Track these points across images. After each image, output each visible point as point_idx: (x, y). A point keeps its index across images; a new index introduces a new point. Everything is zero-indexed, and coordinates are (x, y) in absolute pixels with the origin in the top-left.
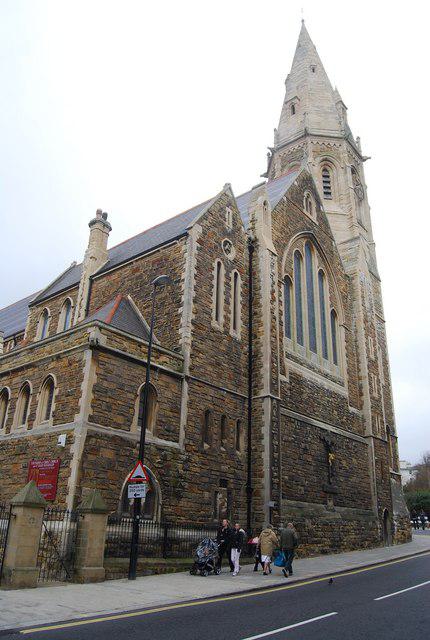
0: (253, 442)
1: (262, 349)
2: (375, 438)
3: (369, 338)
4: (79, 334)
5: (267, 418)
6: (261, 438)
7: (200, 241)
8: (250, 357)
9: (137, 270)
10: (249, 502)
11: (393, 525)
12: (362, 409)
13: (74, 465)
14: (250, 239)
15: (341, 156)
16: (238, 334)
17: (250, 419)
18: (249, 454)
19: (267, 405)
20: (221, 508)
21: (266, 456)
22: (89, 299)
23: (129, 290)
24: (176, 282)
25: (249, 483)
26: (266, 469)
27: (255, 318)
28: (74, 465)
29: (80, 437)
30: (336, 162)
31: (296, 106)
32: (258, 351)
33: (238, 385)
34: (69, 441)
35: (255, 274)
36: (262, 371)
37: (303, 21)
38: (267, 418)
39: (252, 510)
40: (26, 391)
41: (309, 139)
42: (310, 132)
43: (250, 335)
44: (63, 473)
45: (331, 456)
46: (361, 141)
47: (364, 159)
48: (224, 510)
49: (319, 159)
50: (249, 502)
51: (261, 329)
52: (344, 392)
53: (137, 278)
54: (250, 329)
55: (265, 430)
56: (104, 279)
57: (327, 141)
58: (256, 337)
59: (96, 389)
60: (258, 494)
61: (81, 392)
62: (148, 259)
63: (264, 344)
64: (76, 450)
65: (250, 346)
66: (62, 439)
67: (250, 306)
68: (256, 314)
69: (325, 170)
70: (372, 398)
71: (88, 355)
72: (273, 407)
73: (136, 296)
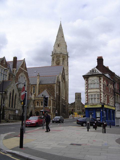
59: (52, 103)
64: (52, 109)
66: (50, 108)
71: (52, 100)
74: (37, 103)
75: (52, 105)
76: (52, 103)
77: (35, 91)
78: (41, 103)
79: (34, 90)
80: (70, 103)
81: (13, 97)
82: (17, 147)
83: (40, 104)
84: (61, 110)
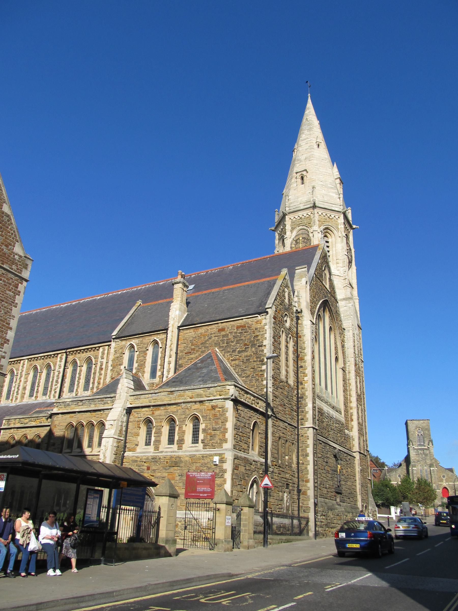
0: (301, 458)
2: (360, 453)
3: (358, 377)
4: (432, 472)
6: (307, 455)
8: (298, 398)
9: (223, 330)
10: (299, 499)
14: (297, 310)
15: (339, 227)
17: (298, 442)
18: (298, 467)
19: (310, 432)
21: (310, 468)
22: (178, 345)
23: (217, 344)
24: (259, 346)
25: (298, 486)
27: (300, 370)
28: (228, 476)
29: (229, 456)
30: (335, 232)
31: (305, 178)
32: (304, 394)
33: (292, 419)
34: (222, 461)
35: (300, 337)
39: (301, 504)
40: (172, 421)
41: (316, 210)
42: (317, 205)
43: (298, 382)
44: (218, 481)
49: (322, 228)
51: (306, 379)
53: (223, 336)
54: (298, 378)
57: (329, 213)
58: (302, 384)
59: (236, 428)
60: (305, 493)
61: (227, 429)
62: (232, 323)
64: (228, 466)
65: (298, 389)
66: (216, 459)
67: (298, 360)
68: (301, 367)
69: (325, 236)
70: (359, 423)
71: (229, 405)
72: (315, 435)
73: (224, 350)
74: (143, 430)
75: (230, 435)
76: (230, 425)
77: (159, 367)
78: (166, 430)
79: (155, 361)
80: (125, 541)
81: (31, 389)
82: (32, 263)
83: (159, 433)
84: (311, 476)
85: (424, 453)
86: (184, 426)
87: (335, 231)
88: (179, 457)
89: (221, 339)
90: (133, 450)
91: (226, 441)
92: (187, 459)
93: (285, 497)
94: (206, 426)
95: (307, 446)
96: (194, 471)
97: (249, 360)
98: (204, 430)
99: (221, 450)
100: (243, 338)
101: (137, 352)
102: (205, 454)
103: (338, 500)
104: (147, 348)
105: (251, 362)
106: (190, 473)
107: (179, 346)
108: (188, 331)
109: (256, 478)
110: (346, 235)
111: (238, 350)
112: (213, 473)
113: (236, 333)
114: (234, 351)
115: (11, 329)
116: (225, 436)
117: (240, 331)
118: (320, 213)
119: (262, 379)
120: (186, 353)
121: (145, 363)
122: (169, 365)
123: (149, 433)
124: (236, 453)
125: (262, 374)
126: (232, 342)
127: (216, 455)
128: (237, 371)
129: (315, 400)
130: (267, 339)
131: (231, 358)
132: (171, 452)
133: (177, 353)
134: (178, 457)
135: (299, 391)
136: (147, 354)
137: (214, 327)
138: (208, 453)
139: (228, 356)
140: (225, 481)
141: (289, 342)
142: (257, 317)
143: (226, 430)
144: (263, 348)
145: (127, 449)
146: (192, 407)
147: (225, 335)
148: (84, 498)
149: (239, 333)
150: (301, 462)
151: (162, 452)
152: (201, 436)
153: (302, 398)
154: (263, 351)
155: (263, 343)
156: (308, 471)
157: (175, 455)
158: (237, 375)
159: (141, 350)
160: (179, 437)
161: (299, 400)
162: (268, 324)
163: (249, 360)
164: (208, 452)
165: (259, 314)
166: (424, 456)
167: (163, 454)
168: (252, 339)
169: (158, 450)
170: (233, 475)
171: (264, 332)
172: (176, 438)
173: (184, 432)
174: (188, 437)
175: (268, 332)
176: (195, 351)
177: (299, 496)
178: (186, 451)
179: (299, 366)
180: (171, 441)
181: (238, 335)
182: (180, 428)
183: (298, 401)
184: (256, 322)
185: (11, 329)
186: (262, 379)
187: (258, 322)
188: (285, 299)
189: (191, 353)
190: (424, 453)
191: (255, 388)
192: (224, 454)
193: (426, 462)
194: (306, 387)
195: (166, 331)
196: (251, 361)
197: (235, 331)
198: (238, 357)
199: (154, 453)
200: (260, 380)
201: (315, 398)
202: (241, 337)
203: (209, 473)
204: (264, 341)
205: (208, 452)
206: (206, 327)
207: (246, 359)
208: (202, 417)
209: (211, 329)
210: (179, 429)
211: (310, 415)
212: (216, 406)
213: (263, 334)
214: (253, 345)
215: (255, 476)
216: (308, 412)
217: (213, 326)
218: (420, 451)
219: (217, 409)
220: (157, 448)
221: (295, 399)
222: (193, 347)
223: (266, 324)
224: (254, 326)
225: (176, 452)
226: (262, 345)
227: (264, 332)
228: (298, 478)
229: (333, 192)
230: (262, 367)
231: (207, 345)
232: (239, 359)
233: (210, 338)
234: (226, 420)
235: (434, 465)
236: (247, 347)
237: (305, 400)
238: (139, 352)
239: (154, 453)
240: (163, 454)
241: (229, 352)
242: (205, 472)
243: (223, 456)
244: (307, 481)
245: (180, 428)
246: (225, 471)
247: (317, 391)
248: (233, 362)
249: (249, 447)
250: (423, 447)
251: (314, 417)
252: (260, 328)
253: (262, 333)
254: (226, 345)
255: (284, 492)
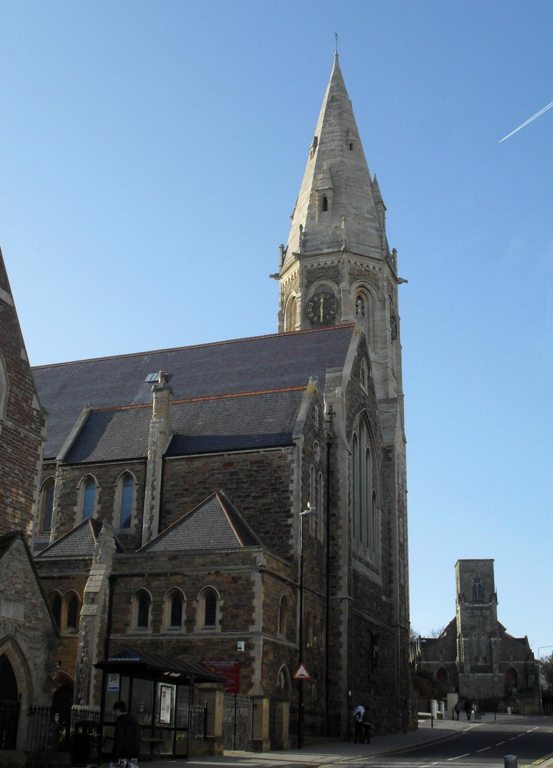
0: (331, 638)
1: (341, 552)
5: (344, 617)
7: (382, 525)
8: (328, 558)
11: (408, 713)
12: (390, 596)
13: (257, 665)
15: (380, 284)
16: (321, 538)
20: (314, 697)
25: (327, 673)
26: (344, 662)
27: (333, 519)
29: (259, 642)
32: (336, 553)
34: (249, 647)
36: (340, 573)
37: (375, 174)
38: (344, 617)
39: (330, 698)
44: (244, 671)
45: (376, 648)
46: (398, 255)
47: (398, 281)
48: (316, 699)
50: (327, 691)
51: (339, 532)
52: (378, 580)
53: (232, 474)
55: (343, 629)
56: (183, 463)
58: (333, 539)
63: (343, 547)
64: (257, 654)
68: (334, 515)
78: (168, 607)
83: (159, 611)
85: (482, 614)
86: (195, 603)
87: (373, 290)
88: (189, 641)
89: (228, 477)
90: (123, 631)
91: (253, 622)
92: (200, 643)
93: (313, 689)
94: (225, 603)
95: (340, 623)
96: (211, 659)
97: (269, 509)
98: (223, 609)
99: (246, 634)
100: (260, 478)
101: (98, 487)
102: (225, 639)
103: (372, 692)
104: (114, 483)
105: (272, 513)
106: (205, 662)
107: (165, 484)
108: (178, 463)
109: (284, 666)
110: (389, 295)
111: (253, 494)
112: (237, 662)
113: (250, 470)
114: (247, 496)
115: (34, 501)
116: (251, 616)
117: (255, 468)
118: (352, 262)
119: (287, 537)
120: (175, 495)
121: (112, 504)
122: (152, 511)
123: (143, 611)
124: (266, 638)
125: (288, 530)
126: (244, 483)
127: (241, 639)
128: (252, 524)
129: (351, 561)
130: (295, 482)
131: (243, 506)
132: (178, 635)
133: (162, 493)
134: (188, 641)
135: (330, 549)
136: (115, 491)
137: (217, 460)
138: (229, 637)
139: (238, 502)
140: (253, 671)
141: (319, 482)
142: (280, 450)
143: (252, 609)
144: (289, 495)
145: (112, 631)
146: (205, 578)
147: (234, 472)
148: (122, 693)
149: (254, 471)
150: (331, 643)
151: (164, 635)
152: (219, 616)
153: (334, 558)
154: (288, 498)
155: (288, 487)
156: (340, 655)
157: (183, 639)
158: (251, 530)
159: (105, 485)
160: (188, 617)
161: (330, 560)
162: (295, 461)
163: (269, 509)
164: (228, 635)
165: (283, 446)
166: (481, 619)
167: (167, 637)
168: (273, 482)
169: (159, 632)
170: (263, 663)
171: (290, 473)
172: (184, 617)
173: (194, 610)
174: (201, 617)
175: (295, 472)
176: (190, 492)
177: (327, 687)
178: (198, 635)
179: (330, 513)
180: (176, 620)
181: (252, 474)
182: (189, 604)
183: (328, 563)
184: (280, 457)
185: (34, 501)
186: (287, 537)
187: (283, 457)
188: (315, 421)
189: (182, 494)
190: (482, 614)
191: (278, 548)
192: (252, 638)
193: (484, 629)
194: (339, 543)
195: (143, 460)
196: (271, 511)
197: (249, 467)
198: (252, 504)
199: (152, 636)
200: (284, 538)
201: (351, 559)
202: (257, 477)
203: (232, 662)
204: (290, 485)
205: (228, 635)
206: (205, 460)
207: (265, 509)
208: (220, 591)
209: (213, 462)
210: (187, 606)
211: (344, 582)
212: (239, 578)
213: (289, 476)
214: (275, 490)
215: (284, 665)
216: (341, 577)
217: (216, 459)
218: (476, 612)
219: (240, 582)
220: (156, 629)
221: (325, 559)
222: (186, 487)
223: (293, 462)
224: (276, 462)
225: (184, 635)
226: (288, 490)
227: (290, 473)
228: (327, 664)
229: (372, 227)
230: (287, 521)
231: (207, 486)
232: (255, 508)
233: (212, 475)
234: (252, 596)
235: (497, 633)
236: (266, 491)
237: (338, 561)
238: (103, 488)
239: (152, 636)
240: (167, 637)
241: (239, 497)
242: (225, 660)
243: (250, 641)
244: (340, 668)
245: (189, 604)
246: (253, 659)
247: (353, 548)
248: (247, 512)
249: (276, 628)
250: (481, 605)
251: (350, 584)
252: (284, 466)
253: (287, 473)
254: (235, 487)
255: (312, 683)
